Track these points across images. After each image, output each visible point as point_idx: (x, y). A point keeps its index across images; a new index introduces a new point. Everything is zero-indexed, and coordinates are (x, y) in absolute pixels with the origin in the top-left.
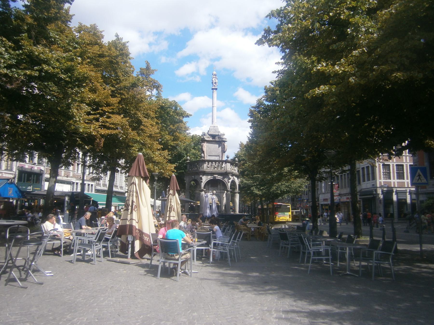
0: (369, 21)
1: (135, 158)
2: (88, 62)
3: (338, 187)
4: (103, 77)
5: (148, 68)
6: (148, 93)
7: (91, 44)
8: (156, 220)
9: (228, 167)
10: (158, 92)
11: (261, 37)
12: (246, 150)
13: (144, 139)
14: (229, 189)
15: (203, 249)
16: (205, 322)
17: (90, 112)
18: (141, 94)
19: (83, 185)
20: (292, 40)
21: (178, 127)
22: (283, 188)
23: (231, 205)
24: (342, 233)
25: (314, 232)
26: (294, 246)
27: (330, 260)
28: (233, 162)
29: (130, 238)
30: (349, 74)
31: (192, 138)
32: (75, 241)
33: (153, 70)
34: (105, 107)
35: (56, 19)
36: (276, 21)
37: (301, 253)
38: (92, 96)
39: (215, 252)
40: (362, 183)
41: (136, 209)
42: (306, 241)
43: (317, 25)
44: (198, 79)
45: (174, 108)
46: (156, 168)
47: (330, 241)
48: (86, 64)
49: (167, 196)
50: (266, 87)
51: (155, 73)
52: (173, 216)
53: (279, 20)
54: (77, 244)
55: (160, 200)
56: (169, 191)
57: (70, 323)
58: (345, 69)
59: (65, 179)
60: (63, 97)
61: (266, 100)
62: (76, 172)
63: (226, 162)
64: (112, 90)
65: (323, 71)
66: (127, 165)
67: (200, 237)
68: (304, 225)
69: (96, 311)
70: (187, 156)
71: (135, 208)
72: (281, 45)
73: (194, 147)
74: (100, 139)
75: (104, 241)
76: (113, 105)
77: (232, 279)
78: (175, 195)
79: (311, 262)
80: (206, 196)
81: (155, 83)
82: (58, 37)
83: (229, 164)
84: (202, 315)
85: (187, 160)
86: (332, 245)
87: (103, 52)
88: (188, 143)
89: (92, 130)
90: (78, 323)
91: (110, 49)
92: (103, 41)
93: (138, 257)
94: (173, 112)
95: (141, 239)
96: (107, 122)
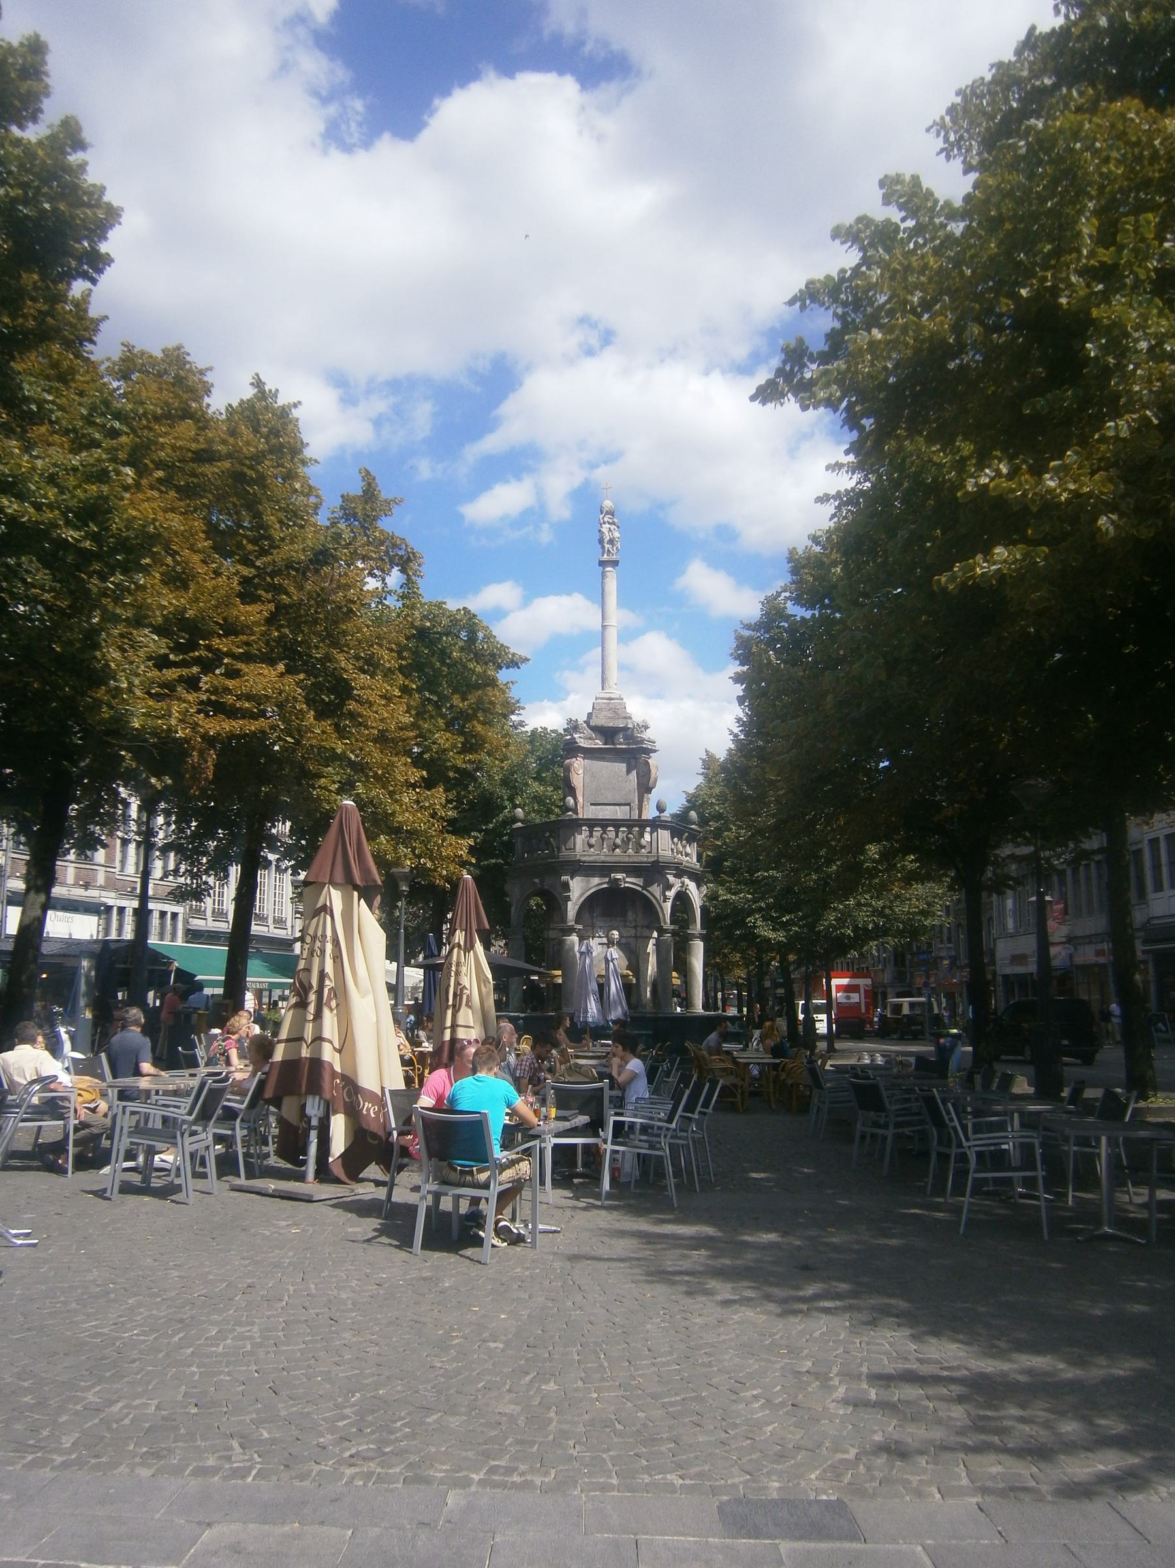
0: (1161, 314)
1: (328, 816)
2: (159, 480)
3: (1065, 912)
4: (212, 530)
5: (370, 493)
6: (372, 584)
7: (167, 416)
8: (402, 1039)
9: (664, 845)
10: (409, 579)
11: (772, 376)
12: (727, 780)
13: (361, 749)
14: (667, 924)
15: (575, 1145)
16: (586, 1417)
17: (167, 656)
18: (347, 587)
19: (142, 915)
20: (884, 386)
21: (480, 701)
22: (863, 917)
23: (676, 982)
24: (1083, 1082)
25: (978, 1078)
26: (907, 1131)
27: (1040, 1181)
28: (679, 827)
29: (313, 1109)
30: (1094, 506)
31: (531, 742)
32: (115, 1117)
33: (388, 502)
34: (220, 636)
35: (42, 335)
36: (823, 321)
37: (934, 1156)
38: (169, 600)
39: (619, 1157)
40: (1151, 895)
41: (333, 1004)
42: (948, 1113)
43: (976, 330)
44: (546, 536)
45: (463, 634)
46: (403, 850)
47: (1039, 1113)
48: (152, 488)
49: (443, 953)
50: (792, 551)
51: (396, 509)
52: (468, 1027)
53: (835, 315)
54: (125, 1130)
55: (419, 966)
56: (452, 932)
57: (96, 1421)
58: (1081, 486)
59: (78, 893)
60: (69, 607)
61: (798, 600)
62: (117, 870)
63: (656, 824)
64: (243, 577)
65: (1000, 496)
66: (298, 840)
67: (565, 1100)
68: (944, 1054)
69: (194, 1374)
70: (515, 806)
71: (329, 999)
72: (844, 404)
73: (538, 773)
74: (201, 753)
75: (218, 1119)
76: (245, 629)
77: (685, 1257)
78: (472, 947)
79: (968, 1193)
80: (583, 949)
81: (394, 546)
82: (50, 398)
83: (664, 835)
84: (576, 1390)
85: (515, 820)
86: (1045, 1129)
87: (210, 441)
88: (515, 759)
89: (173, 722)
90: (127, 1421)
91: (233, 433)
92: (209, 405)
93: (343, 1177)
94: (462, 649)
95: (353, 1113)
96: (227, 690)
